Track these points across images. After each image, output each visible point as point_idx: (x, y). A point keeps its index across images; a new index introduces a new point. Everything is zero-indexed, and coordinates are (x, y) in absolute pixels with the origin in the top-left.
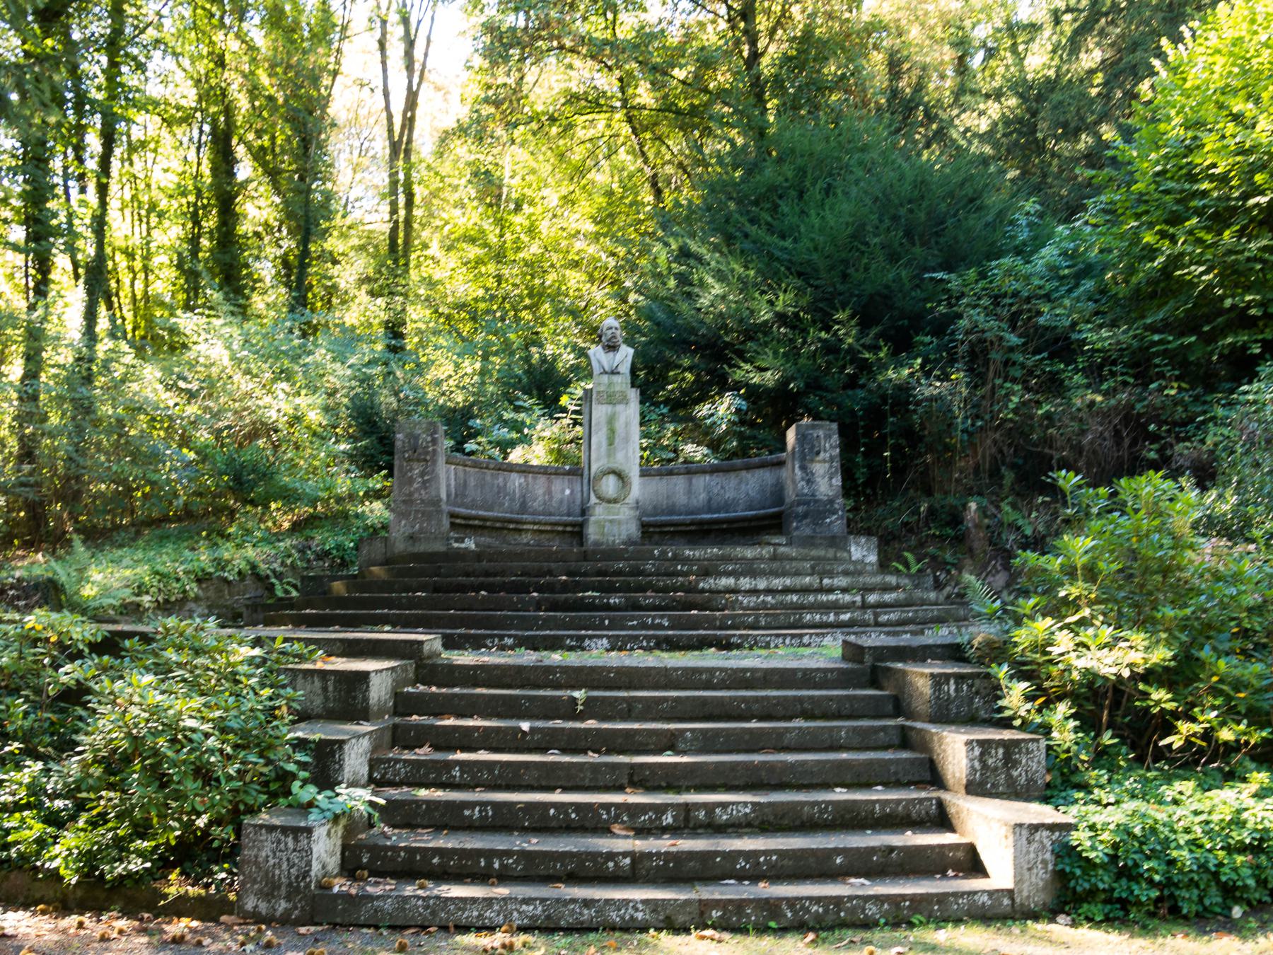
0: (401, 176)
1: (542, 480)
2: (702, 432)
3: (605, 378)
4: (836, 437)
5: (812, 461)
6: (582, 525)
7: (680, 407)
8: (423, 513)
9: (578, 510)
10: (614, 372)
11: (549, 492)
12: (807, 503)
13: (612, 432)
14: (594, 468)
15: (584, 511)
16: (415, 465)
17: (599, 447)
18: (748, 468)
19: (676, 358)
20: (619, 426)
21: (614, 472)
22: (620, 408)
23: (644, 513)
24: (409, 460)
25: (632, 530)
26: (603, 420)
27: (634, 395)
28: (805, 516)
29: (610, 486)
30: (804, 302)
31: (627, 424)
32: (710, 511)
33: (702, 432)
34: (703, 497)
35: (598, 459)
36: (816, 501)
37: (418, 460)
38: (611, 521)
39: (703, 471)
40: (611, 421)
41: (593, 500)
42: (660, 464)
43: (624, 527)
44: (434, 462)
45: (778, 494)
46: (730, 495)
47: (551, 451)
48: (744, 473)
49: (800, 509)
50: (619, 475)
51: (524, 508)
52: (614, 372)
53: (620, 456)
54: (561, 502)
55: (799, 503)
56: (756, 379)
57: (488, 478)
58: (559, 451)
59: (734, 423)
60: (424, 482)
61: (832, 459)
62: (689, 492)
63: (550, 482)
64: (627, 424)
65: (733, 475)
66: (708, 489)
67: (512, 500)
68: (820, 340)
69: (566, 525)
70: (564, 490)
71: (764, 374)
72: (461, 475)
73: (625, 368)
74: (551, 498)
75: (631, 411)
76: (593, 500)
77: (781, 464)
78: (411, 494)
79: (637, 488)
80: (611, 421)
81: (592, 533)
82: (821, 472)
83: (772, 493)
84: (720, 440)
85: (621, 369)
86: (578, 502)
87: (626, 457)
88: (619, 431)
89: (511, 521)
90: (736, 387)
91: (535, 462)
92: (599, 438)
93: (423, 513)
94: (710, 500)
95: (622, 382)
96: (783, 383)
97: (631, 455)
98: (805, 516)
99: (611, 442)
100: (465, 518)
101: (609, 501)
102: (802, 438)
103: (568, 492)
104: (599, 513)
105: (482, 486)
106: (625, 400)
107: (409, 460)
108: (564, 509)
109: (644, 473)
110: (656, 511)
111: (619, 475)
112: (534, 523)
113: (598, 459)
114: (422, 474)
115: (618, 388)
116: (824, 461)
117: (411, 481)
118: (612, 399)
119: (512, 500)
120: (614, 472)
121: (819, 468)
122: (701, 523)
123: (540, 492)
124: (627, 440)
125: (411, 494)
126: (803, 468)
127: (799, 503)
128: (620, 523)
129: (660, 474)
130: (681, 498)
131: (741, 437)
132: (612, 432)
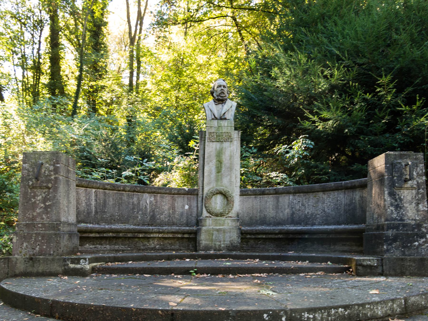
0: (135, 53)
1: (168, 198)
2: (281, 164)
3: (215, 123)
4: (422, 166)
5: (401, 188)
6: (196, 233)
7: (262, 149)
8: (43, 236)
9: (194, 221)
10: (222, 118)
11: (173, 207)
12: (396, 227)
13: (220, 162)
14: (206, 190)
15: (198, 222)
16: (38, 192)
17: (210, 172)
18: (324, 190)
19: (264, 117)
20: (225, 158)
21: (221, 193)
22: (226, 145)
23: (243, 224)
24: (33, 187)
25: (234, 237)
26: (214, 154)
27: (236, 136)
28: (395, 239)
29: (217, 203)
30: (352, 74)
31: (231, 157)
32: (293, 222)
33: (281, 164)
34: (287, 211)
35: (209, 183)
36: (405, 225)
37: (41, 188)
38: (218, 230)
39: (287, 192)
40: (219, 154)
41: (205, 213)
42: (253, 185)
43: (228, 235)
44: (56, 189)
45: (356, 214)
46: (309, 210)
47: (184, 176)
48: (321, 194)
49: (390, 233)
50: (225, 195)
51: (153, 221)
52: (222, 118)
53: (225, 181)
54: (182, 214)
55: (389, 227)
56: (320, 127)
57: (125, 198)
58: (189, 175)
59: (305, 157)
60: (46, 207)
61: (419, 186)
62: (277, 207)
63: (174, 200)
64: (231, 157)
65: (311, 196)
66: (291, 206)
67: (144, 214)
68: (365, 100)
69: (184, 233)
70: (184, 206)
71: (327, 121)
72: (101, 196)
73: (230, 115)
74: (174, 213)
75: (233, 148)
76: (205, 213)
77: (364, 186)
78: (33, 219)
79: (238, 204)
80: (219, 154)
81: (204, 239)
82: (409, 198)
83: (345, 211)
84: (292, 169)
85: (228, 116)
86: (194, 214)
87: (231, 182)
88: (226, 161)
89: (140, 232)
90: (304, 131)
91: (173, 185)
92: (210, 167)
93: (43, 236)
94: (293, 214)
95: (228, 126)
96: (339, 129)
97: (233, 182)
98: (395, 239)
99: (219, 170)
100: (98, 232)
101: (217, 215)
102: (391, 166)
103: (187, 207)
104: (209, 223)
105: (120, 204)
106: (229, 139)
107: (33, 187)
108: (184, 220)
109: (244, 193)
110: (252, 222)
111: (225, 195)
112: (159, 233)
113: (209, 183)
114: (44, 200)
115: (224, 130)
116: (412, 188)
117: (34, 206)
118: (220, 138)
119: (144, 214)
120: (221, 193)
121: (407, 195)
122: (288, 233)
123: (166, 207)
124: (231, 169)
125: (33, 219)
126: (392, 194)
127: (389, 227)
128: (224, 231)
129: (255, 194)
130: (271, 213)
131: (308, 167)
132: (220, 162)
